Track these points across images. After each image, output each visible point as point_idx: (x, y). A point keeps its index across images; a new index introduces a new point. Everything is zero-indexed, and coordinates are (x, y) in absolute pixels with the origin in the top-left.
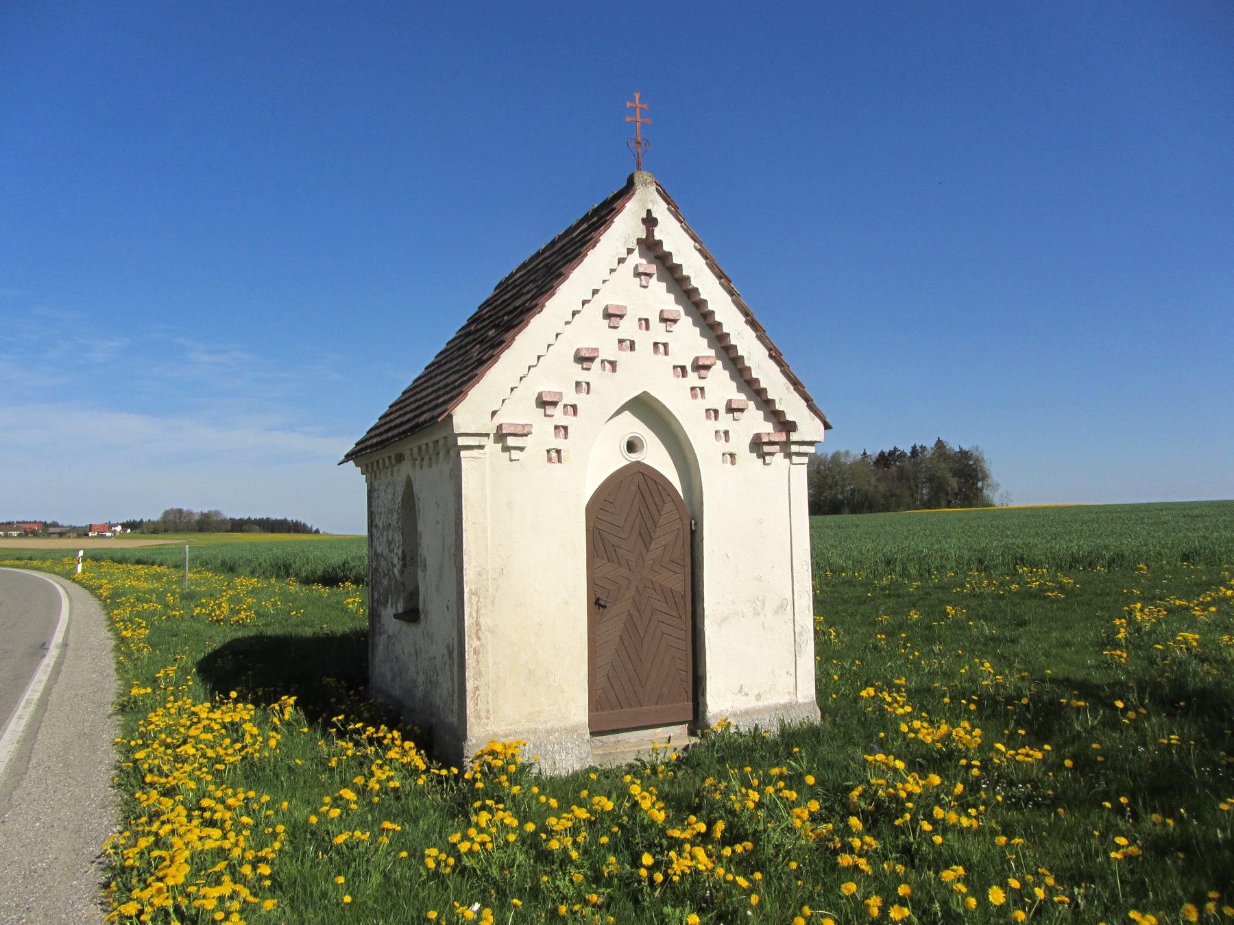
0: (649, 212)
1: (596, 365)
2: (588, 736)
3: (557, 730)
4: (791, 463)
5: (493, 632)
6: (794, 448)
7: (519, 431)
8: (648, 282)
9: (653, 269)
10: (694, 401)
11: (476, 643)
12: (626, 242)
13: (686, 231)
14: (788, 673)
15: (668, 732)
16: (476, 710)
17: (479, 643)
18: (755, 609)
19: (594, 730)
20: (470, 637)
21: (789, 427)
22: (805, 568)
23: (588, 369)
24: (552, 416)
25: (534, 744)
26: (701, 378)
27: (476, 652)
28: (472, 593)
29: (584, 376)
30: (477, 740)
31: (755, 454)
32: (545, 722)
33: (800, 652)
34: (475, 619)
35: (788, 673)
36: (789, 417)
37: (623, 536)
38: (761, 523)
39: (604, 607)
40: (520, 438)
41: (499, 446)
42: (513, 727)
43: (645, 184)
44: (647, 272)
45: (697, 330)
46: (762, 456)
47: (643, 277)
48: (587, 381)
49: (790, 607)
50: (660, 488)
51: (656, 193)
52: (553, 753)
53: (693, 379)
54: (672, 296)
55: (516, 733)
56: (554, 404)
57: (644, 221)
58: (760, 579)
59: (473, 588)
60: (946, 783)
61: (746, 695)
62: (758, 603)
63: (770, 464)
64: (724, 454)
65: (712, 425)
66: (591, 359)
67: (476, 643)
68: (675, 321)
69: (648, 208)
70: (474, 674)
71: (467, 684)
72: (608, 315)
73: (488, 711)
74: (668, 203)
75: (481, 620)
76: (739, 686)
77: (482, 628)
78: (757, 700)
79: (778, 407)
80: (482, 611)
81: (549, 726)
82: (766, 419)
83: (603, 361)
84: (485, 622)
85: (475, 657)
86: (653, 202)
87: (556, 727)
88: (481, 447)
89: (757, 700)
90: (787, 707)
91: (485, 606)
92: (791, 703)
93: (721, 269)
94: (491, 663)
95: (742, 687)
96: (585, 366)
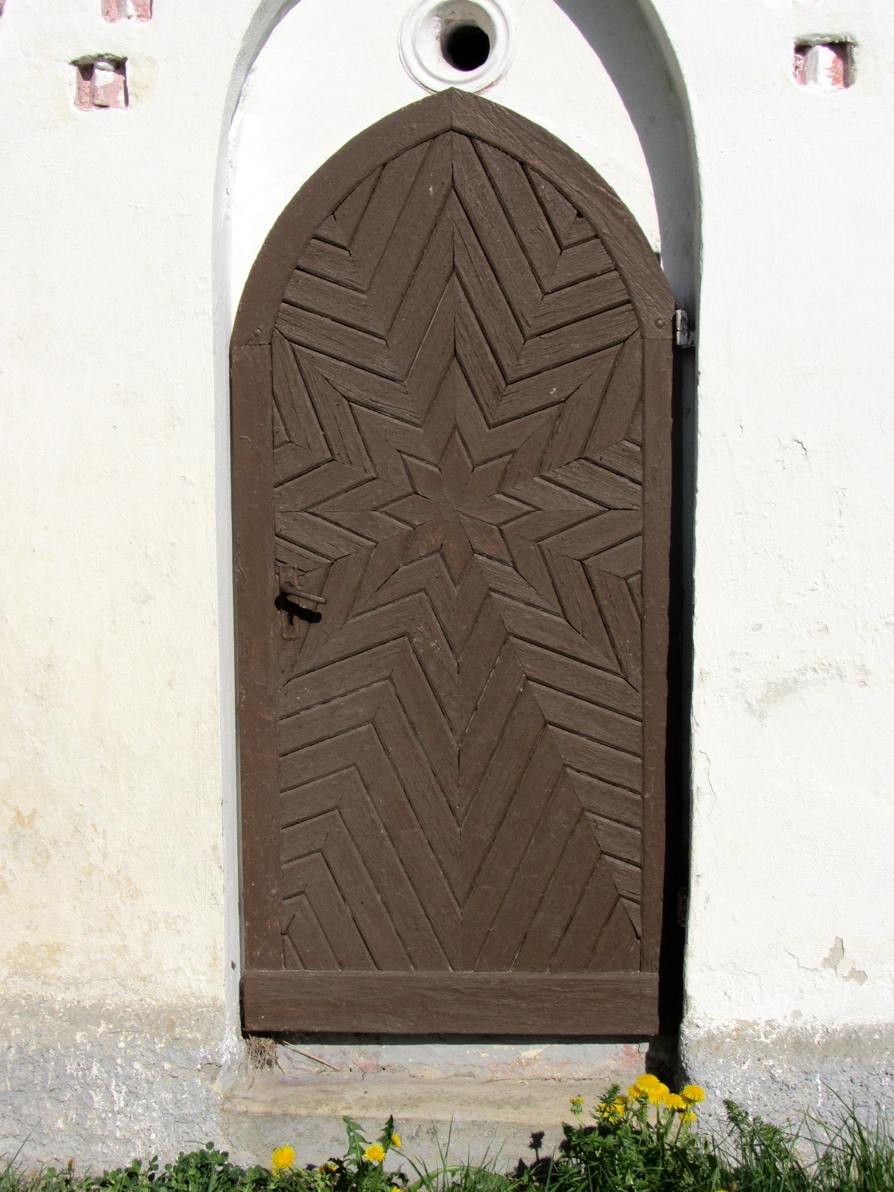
3: (109, 1017)
19: (638, 966)
25: (20, 1050)
32: (76, 983)
37: (387, 366)
39: (312, 617)
50: (544, 188)
52: (87, 1085)
61: (860, 976)
64: (802, 48)
76: (831, 943)
81: (89, 996)
87: (111, 1004)
95: (839, 948)
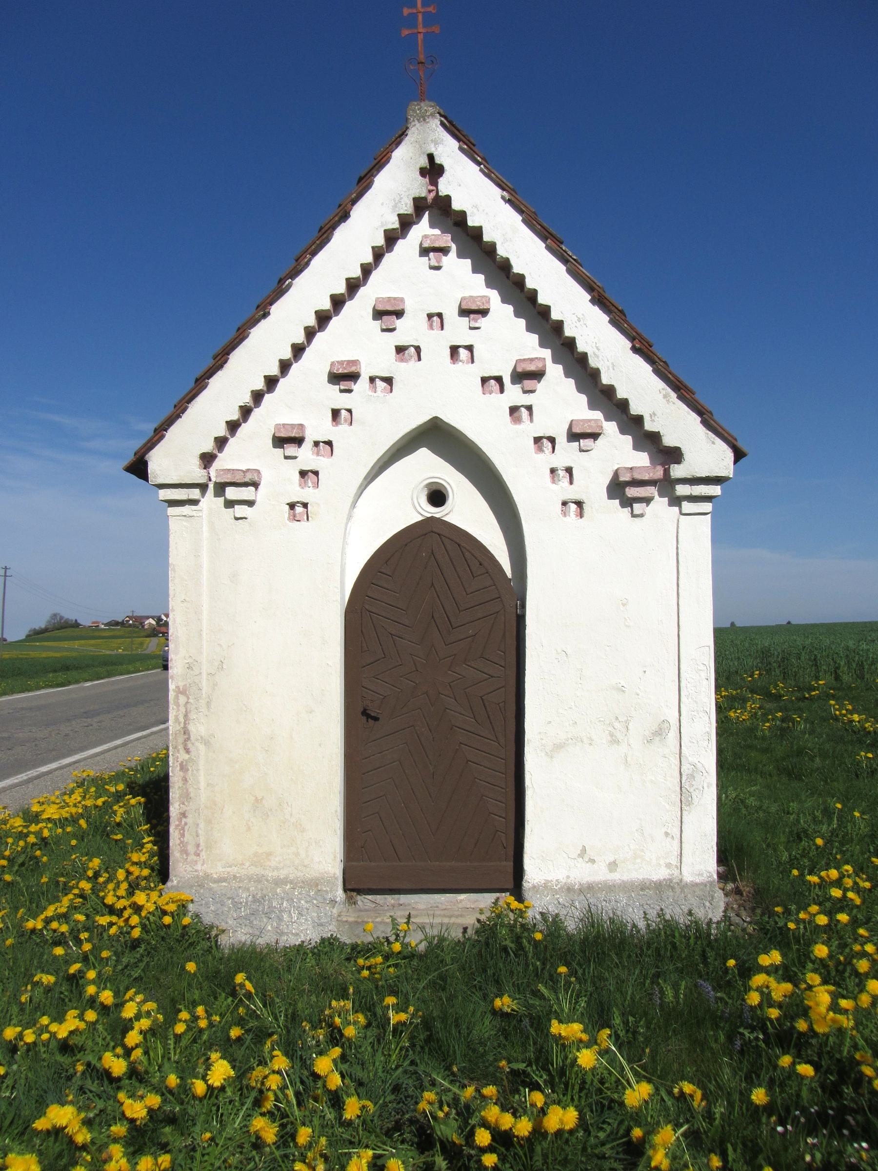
0: (431, 157)
1: (362, 384)
2: (340, 894)
3: (291, 882)
4: (681, 514)
5: (207, 743)
6: (682, 490)
7: (238, 479)
8: (439, 261)
9: (446, 240)
10: (517, 427)
11: (183, 756)
12: (395, 206)
13: (488, 176)
14: (667, 834)
15: (476, 901)
16: (182, 842)
17: (187, 757)
18: (611, 735)
20: (175, 748)
21: (674, 455)
22: (703, 675)
23: (349, 391)
24: (295, 458)
25: (254, 897)
26: (525, 392)
27: (183, 768)
28: (180, 692)
29: (342, 401)
30: (179, 882)
31: (617, 501)
32: (277, 869)
33: (689, 804)
34: (182, 725)
35: (667, 834)
36: (669, 441)
38: (624, 605)
40: (244, 488)
41: (221, 500)
42: (234, 870)
43: (423, 118)
44: (437, 245)
45: (522, 322)
46: (628, 503)
47: (431, 254)
48: (348, 407)
49: (673, 735)
50: (467, 554)
51: (441, 129)
52: (281, 911)
53: (514, 394)
54: (481, 278)
55: (235, 877)
56: (298, 441)
57: (423, 172)
58: (621, 690)
59: (181, 684)
60: (71, 1098)
61: (592, 861)
62: (617, 725)
63: (641, 516)
65: (546, 459)
66: (353, 377)
67: (183, 756)
68: (484, 312)
69: (429, 152)
70: (181, 796)
71: (171, 809)
72: (379, 314)
73: (198, 846)
74: (459, 140)
75: (191, 728)
77: (192, 738)
78: (611, 871)
79: (649, 426)
80: (192, 716)
81: (282, 874)
82: (637, 447)
83: (372, 380)
84: (197, 729)
85: (182, 774)
86: (436, 143)
87: (291, 877)
88: (194, 502)
89: (611, 871)
90: (660, 887)
91: (196, 708)
92: (671, 880)
93: (545, 225)
94: (202, 785)
96: (342, 387)
